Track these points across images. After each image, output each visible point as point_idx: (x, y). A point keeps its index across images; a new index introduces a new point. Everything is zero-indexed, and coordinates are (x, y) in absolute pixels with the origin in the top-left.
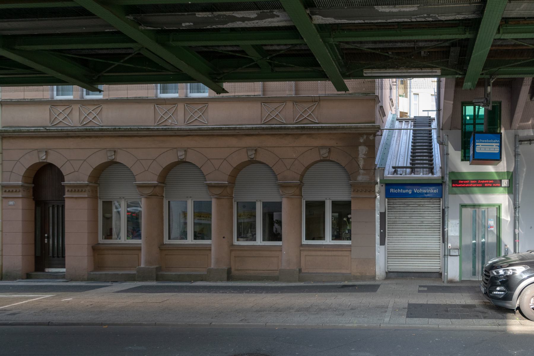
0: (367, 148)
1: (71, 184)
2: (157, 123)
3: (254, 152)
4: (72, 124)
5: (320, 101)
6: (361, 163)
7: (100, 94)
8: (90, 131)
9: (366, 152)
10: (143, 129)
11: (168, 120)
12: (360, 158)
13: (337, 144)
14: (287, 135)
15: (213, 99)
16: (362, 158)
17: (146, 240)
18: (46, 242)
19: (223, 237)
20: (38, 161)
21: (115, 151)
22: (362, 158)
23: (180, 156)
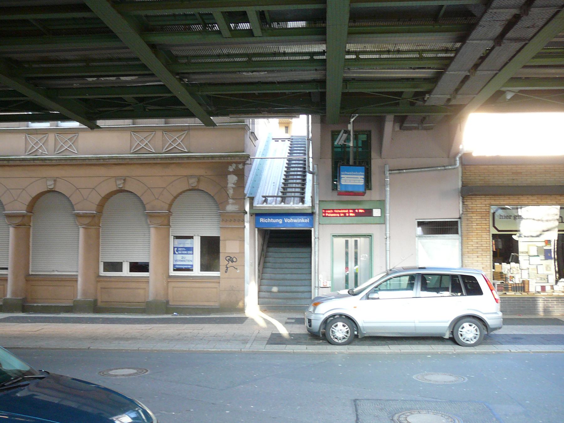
21: (124, 180)
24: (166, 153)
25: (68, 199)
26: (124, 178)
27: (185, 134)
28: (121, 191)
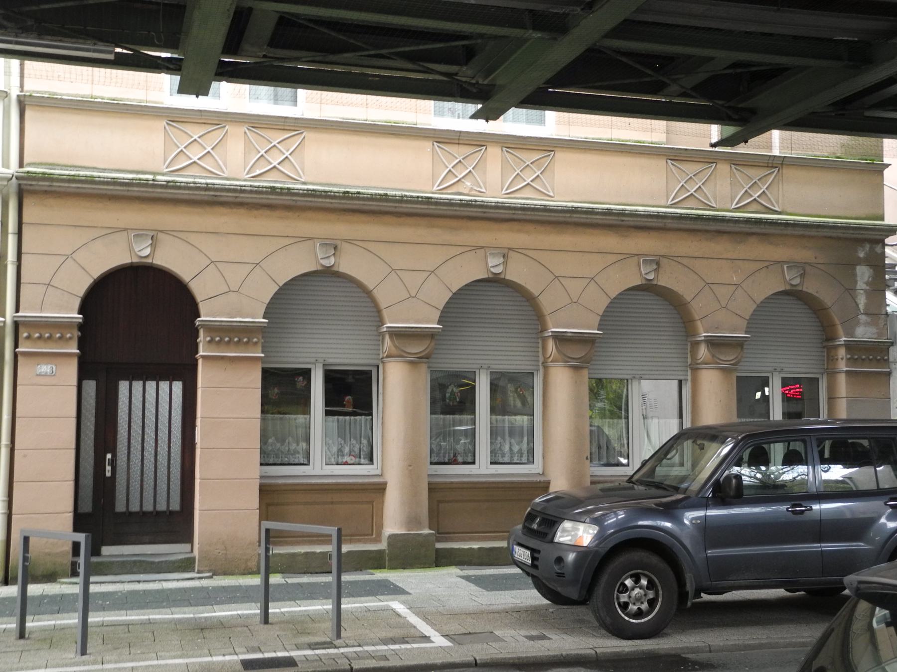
0: (871, 270)
1: (223, 324)
2: (438, 186)
3: (655, 267)
4: (224, 172)
5: (782, 167)
6: (862, 301)
7: (746, 146)
8: (281, 194)
9: (870, 279)
10: (416, 199)
11: (463, 180)
12: (859, 291)
13: (816, 258)
14: (720, 232)
15: (570, 143)
16: (862, 290)
17: (410, 466)
18: (108, 474)
19: (585, 458)
20: (129, 261)
21: (335, 248)
22: (862, 290)
23: (493, 267)
24: (737, 210)
25: (368, 293)
26: (151, 234)
27: (776, 172)
28: (495, 281)
